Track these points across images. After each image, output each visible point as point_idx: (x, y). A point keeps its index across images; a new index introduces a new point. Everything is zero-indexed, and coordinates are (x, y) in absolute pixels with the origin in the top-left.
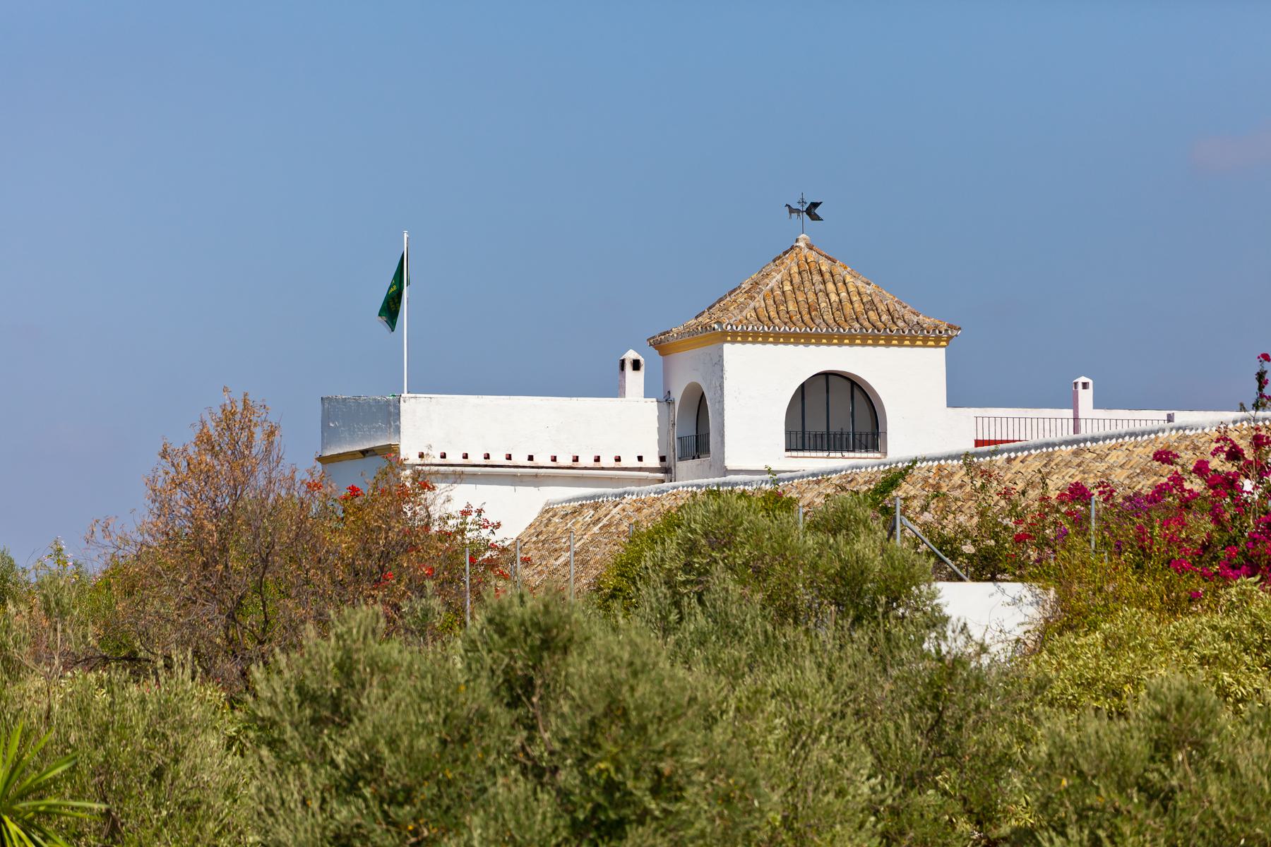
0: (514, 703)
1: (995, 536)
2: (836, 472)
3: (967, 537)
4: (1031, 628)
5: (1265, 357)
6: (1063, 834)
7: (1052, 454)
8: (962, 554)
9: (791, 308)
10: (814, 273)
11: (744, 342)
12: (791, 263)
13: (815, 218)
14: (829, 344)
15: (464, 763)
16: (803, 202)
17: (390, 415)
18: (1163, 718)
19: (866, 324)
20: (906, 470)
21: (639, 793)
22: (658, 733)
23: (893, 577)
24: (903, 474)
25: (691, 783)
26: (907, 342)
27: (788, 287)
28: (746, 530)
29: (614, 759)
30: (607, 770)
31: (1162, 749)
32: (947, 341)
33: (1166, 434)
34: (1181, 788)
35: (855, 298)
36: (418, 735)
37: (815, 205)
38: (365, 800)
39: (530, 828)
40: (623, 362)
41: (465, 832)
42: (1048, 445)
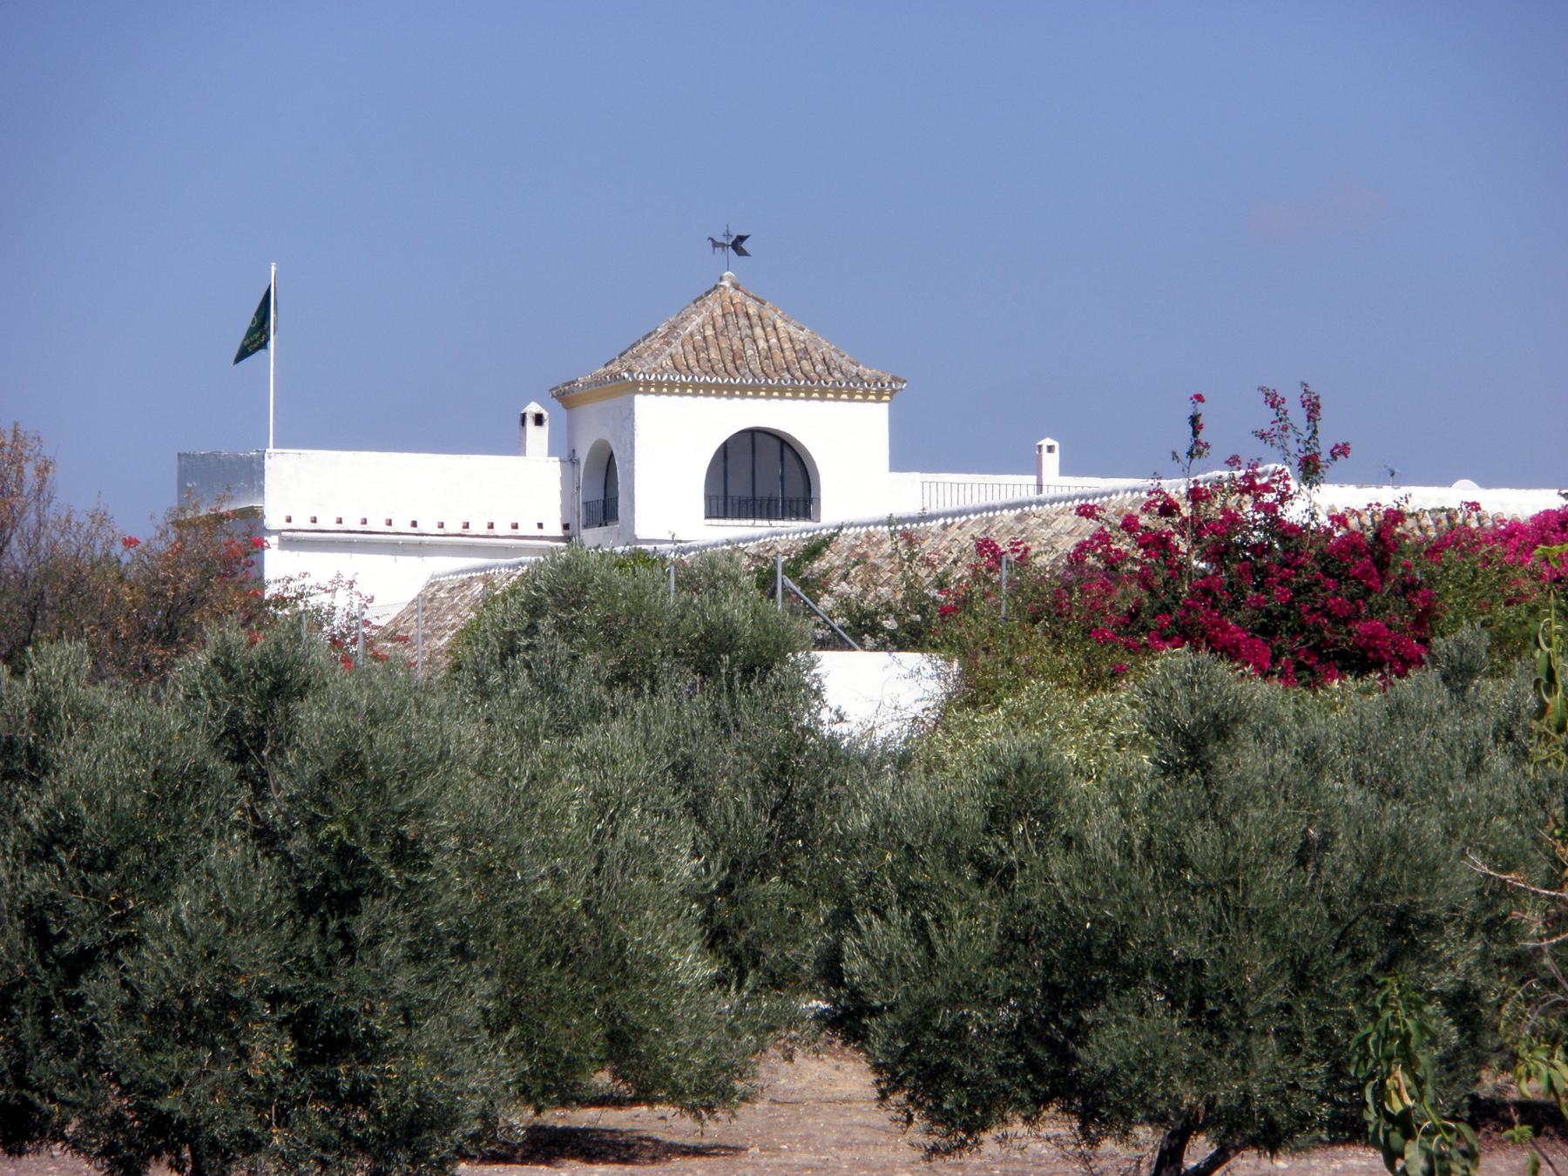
0: (240, 757)
1: (922, 611)
2: (753, 539)
3: (890, 610)
4: (931, 705)
7: (992, 519)
8: (883, 630)
9: (713, 356)
10: (741, 315)
11: (658, 393)
12: (713, 305)
14: (756, 396)
15: (177, 825)
16: (728, 235)
17: (251, 473)
19: (798, 374)
20: (831, 537)
21: (377, 861)
22: (400, 791)
23: (765, 643)
24: (826, 542)
25: (438, 849)
26: (844, 396)
27: (709, 332)
28: (596, 587)
30: (338, 832)
31: (998, 819)
32: (891, 395)
33: (1120, 496)
34: (1022, 865)
35: (787, 346)
36: (124, 790)
37: (742, 239)
38: (61, 867)
39: (247, 899)
40: (524, 417)
41: (173, 903)
42: (988, 509)
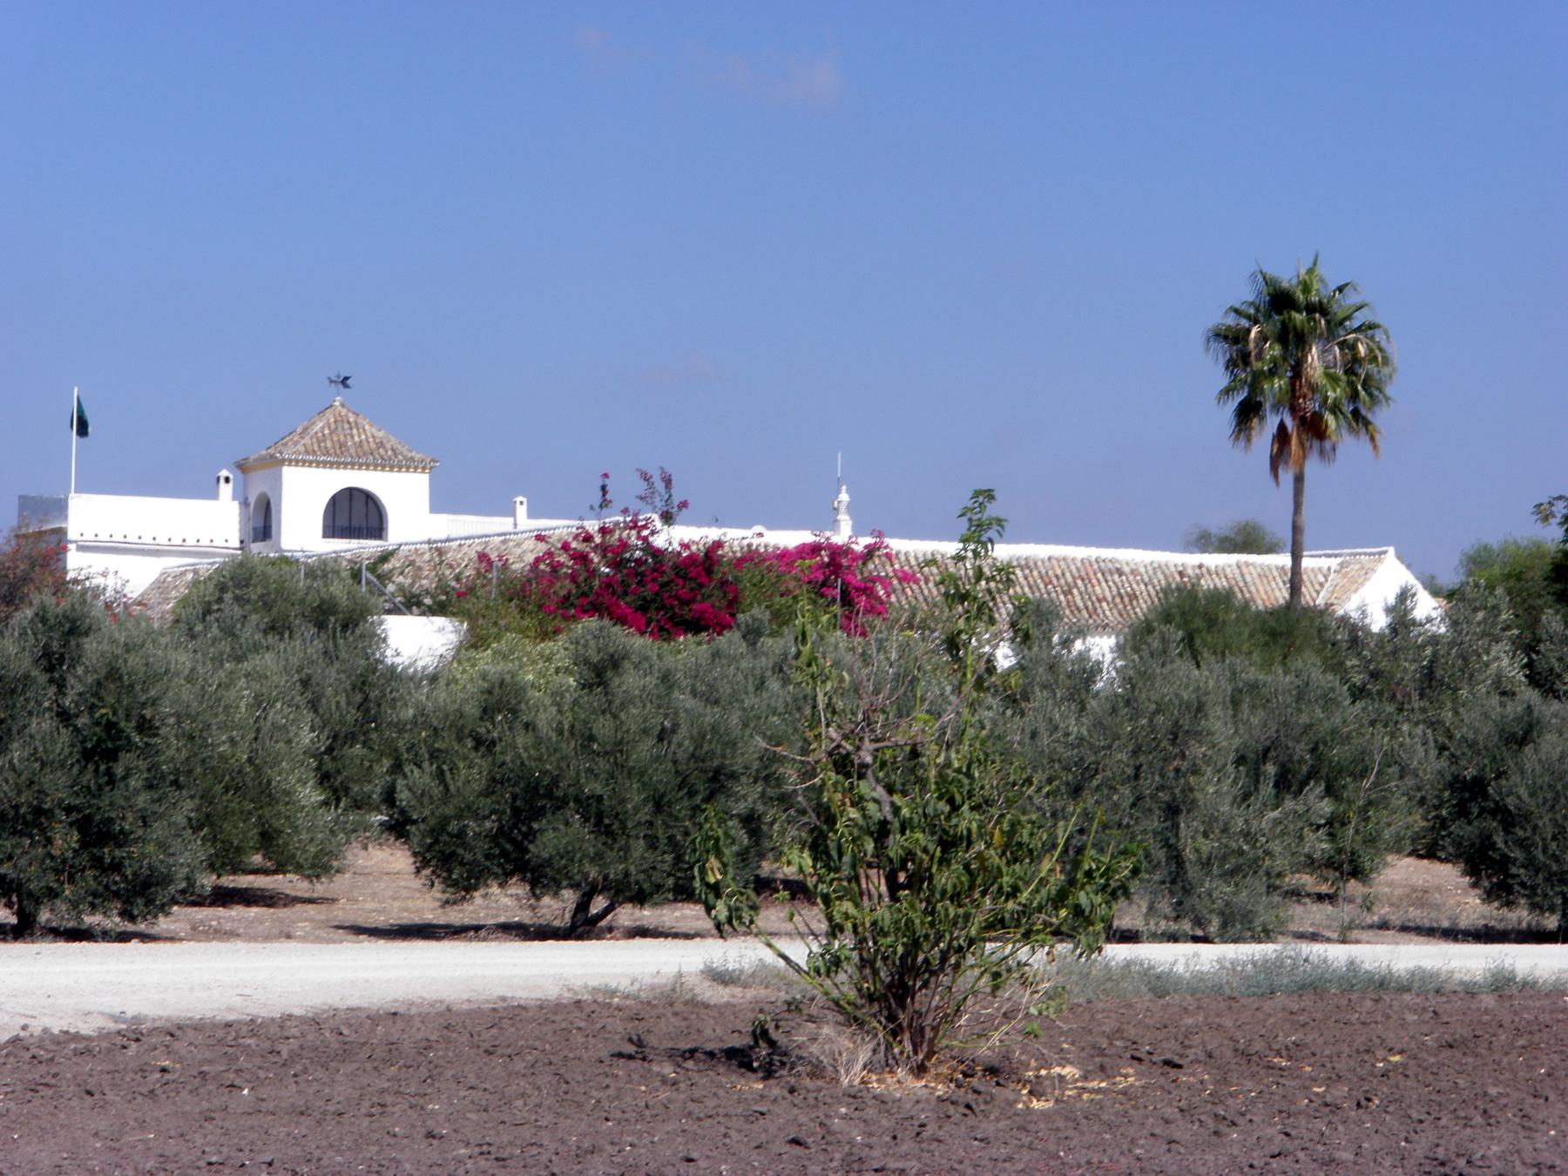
0: (50, 669)
1: (447, 593)
5: (606, 476)
6: (420, 767)
13: (346, 386)
18: (490, 693)
29: (112, 707)
37: (346, 378)
